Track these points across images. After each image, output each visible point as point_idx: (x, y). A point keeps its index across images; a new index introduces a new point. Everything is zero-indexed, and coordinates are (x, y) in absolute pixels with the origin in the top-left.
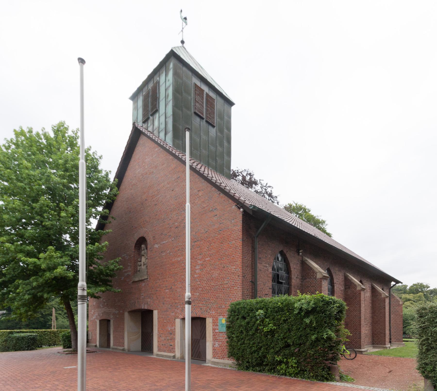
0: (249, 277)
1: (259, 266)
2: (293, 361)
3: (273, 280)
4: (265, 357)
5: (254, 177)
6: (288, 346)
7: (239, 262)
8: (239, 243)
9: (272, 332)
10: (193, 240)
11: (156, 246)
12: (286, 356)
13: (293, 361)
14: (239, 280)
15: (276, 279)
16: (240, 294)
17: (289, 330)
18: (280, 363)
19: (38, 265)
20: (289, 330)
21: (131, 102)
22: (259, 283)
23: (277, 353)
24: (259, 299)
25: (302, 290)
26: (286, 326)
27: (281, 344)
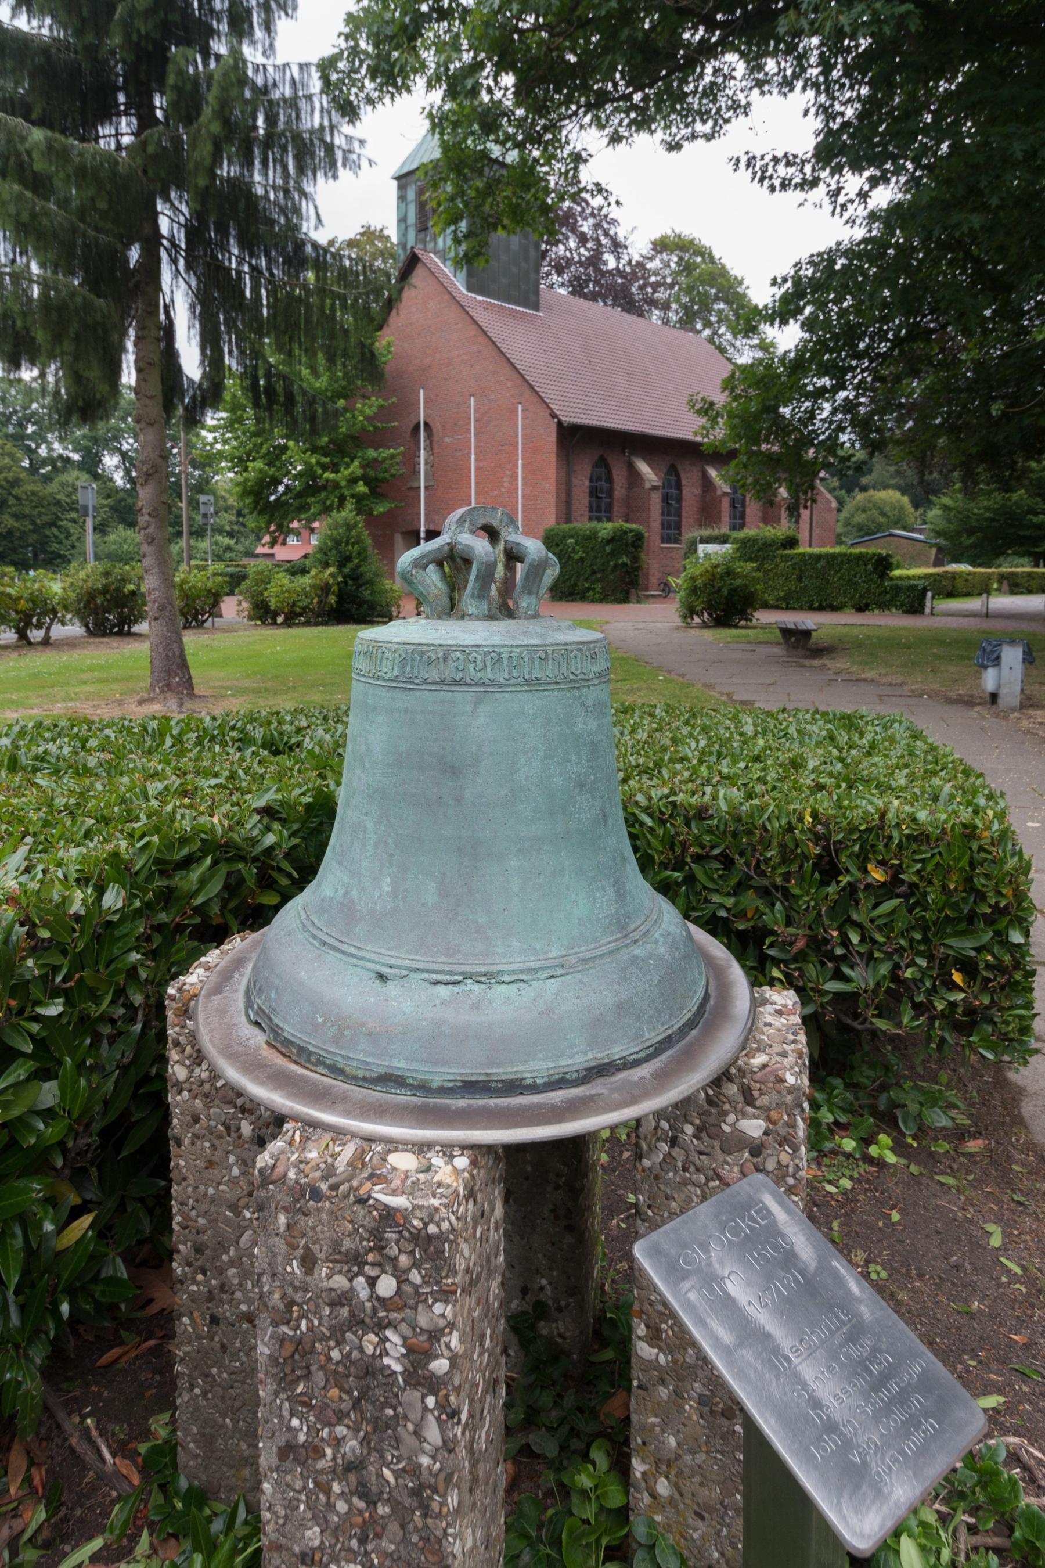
0: (563, 495)
1: (575, 481)
2: (598, 587)
3: (591, 495)
4: (576, 585)
5: (644, 252)
6: (594, 572)
7: (553, 480)
8: (553, 457)
9: (582, 559)
10: (477, 483)
11: (447, 440)
12: (593, 583)
13: (598, 587)
14: (553, 501)
15: (594, 492)
16: (553, 517)
17: (596, 557)
18: (588, 589)
19: (42, 1373)
20: (596, 557)
21: (395, 183)
22: (574, 501)
23: (586, 580)
24: (572, 525)
25: (109, 1227)
26: (592, 554)
27: (589, 571)
